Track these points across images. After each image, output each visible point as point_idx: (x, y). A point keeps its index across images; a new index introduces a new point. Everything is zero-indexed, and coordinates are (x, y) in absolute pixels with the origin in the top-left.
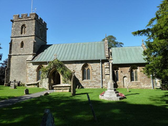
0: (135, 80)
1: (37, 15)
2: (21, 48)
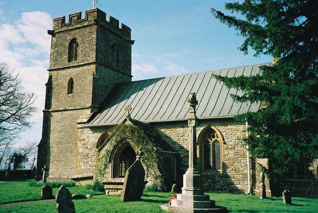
0: (296, 176)
1: (101, 14)
2: (70, 95)
